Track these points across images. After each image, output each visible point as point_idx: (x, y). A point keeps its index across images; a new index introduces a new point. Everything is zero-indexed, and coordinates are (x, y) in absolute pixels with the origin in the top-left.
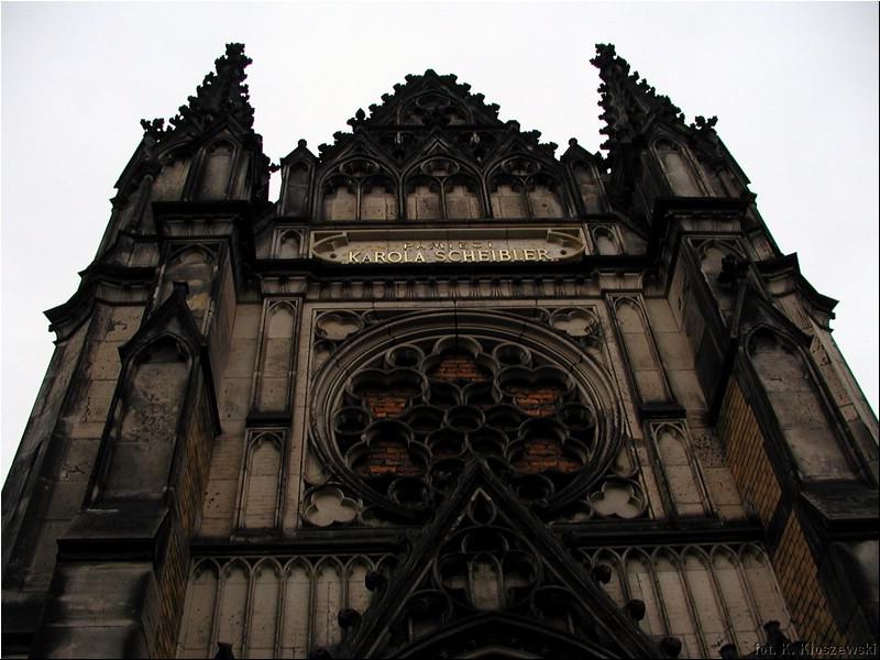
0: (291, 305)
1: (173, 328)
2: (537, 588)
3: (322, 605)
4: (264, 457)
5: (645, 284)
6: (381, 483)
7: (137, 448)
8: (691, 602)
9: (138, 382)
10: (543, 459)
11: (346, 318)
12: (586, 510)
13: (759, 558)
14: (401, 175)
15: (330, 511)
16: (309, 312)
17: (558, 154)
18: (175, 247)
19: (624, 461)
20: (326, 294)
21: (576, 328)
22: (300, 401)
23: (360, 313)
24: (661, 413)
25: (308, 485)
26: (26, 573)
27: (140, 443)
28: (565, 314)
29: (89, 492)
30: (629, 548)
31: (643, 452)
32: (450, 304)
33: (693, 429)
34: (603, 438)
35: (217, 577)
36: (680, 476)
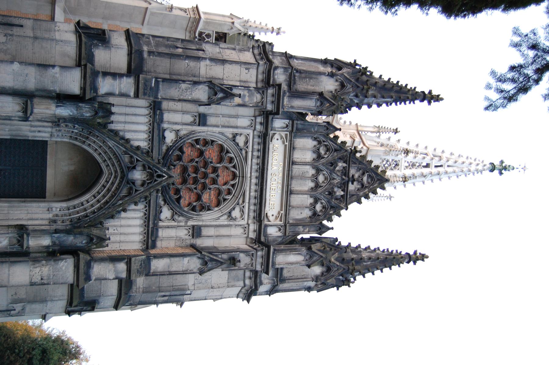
0: (252, 126)
1: (220, 95)
2: (134, 187)
3: (137, 134)
4: (189, 118)
5: (252, 238)
6: (181, 150)
7: (176, 89)
8: (129, 226)
9: (201, 87)
10: (187, 197)
11: (246, 142)
12: (164, 205)
13: (141, 246)
14: (320, 164)
15: (170, 137)
16: (250, 132)
17: (325, 222)
18: (263, 92)
19: (181, 218)
20: (256, 137)
21: (236, 213)
22: (210, 129)
23: (247, 147)
24: (196, 232)
25: (178, 131)
26: (153, 56)
27: (178, 89)
28: (242, 211)
29: (160, 78)
30: (147, 213)
31: (183, 224)
32: (249, 175)
33: (190, 240)
34: (191, 214)
35: (148, 107)
36: (172, 233)
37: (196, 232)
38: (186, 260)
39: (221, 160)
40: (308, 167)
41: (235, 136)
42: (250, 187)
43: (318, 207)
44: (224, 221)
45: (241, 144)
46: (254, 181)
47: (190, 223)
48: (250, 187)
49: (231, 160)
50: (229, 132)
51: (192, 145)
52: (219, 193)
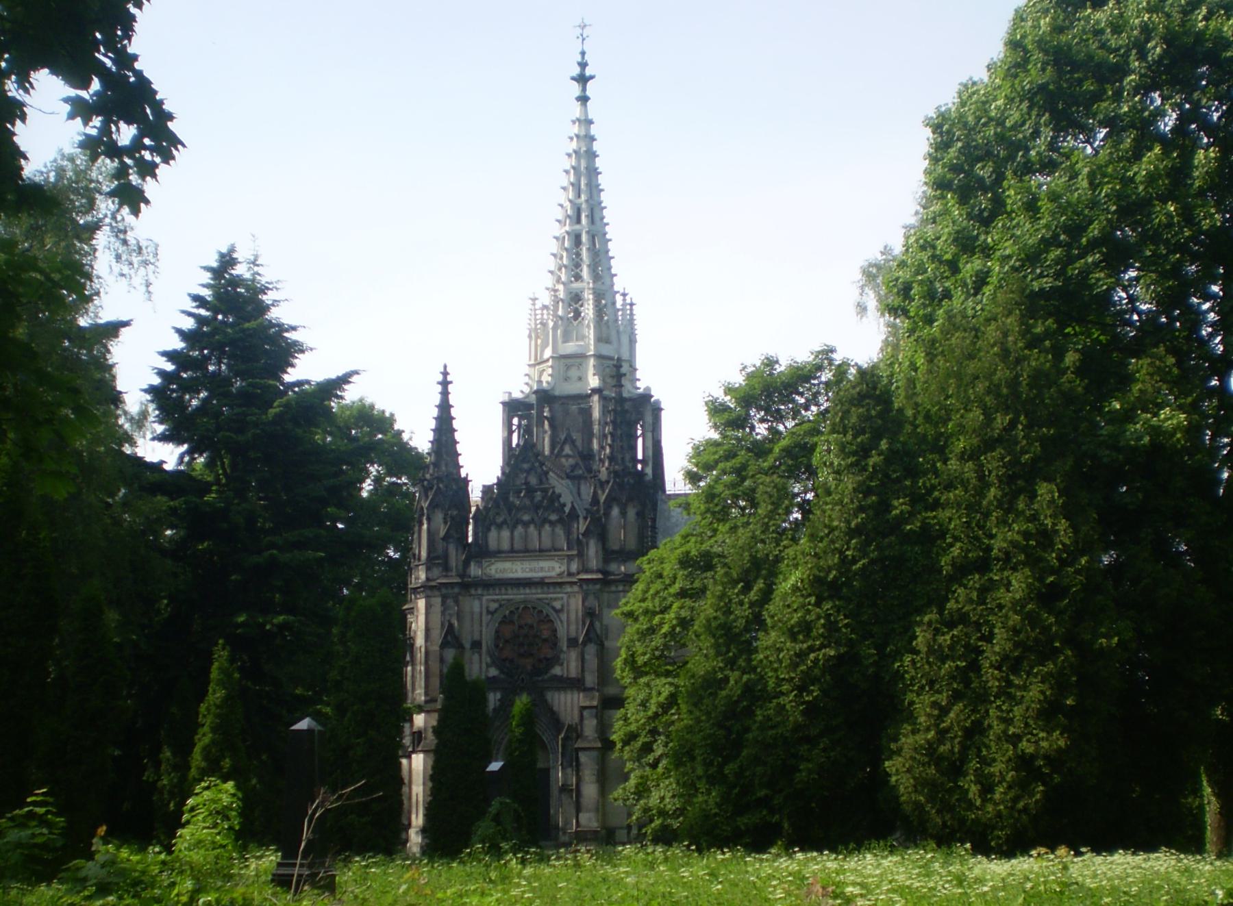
0: (480, 597)
6: (504, 660)
10: (547, 652)
15: (493, 672)
16: (485, 598)
24: (573, 642)
28: (555, 599)
37: (573, 642)
38: (587, 657)
39: (512, 622)
40: (516, 533)
41: (489, 612)
42: (536, 594)
43: (554, 517)
44: (564, 617)
45: (495, 605)
46: (528, 591)
47: (565, 649)
48: (536, 594)
49: (511, 612)
50: (486, 618)
51: (502, 649)
52: (541, 621)
